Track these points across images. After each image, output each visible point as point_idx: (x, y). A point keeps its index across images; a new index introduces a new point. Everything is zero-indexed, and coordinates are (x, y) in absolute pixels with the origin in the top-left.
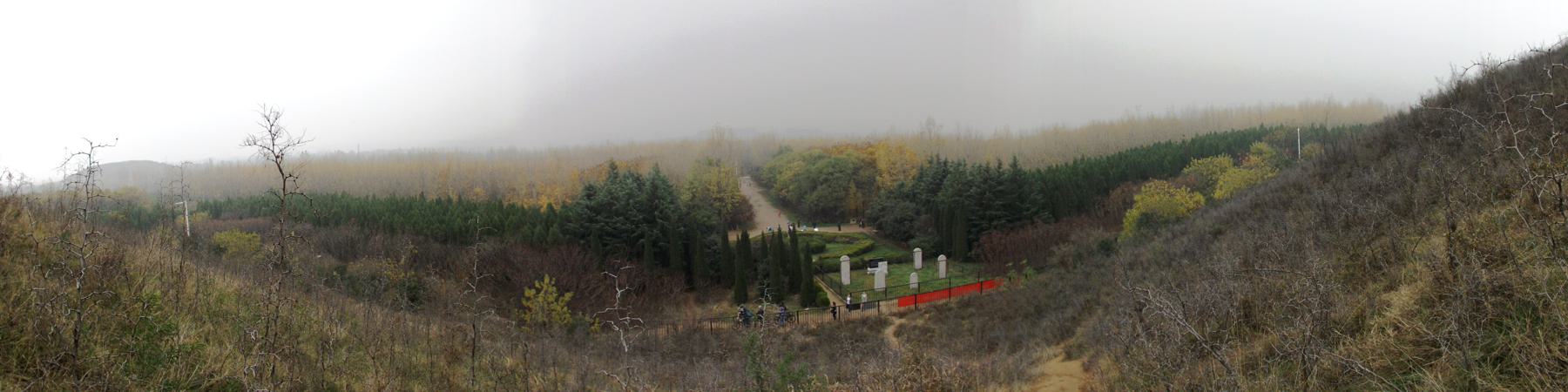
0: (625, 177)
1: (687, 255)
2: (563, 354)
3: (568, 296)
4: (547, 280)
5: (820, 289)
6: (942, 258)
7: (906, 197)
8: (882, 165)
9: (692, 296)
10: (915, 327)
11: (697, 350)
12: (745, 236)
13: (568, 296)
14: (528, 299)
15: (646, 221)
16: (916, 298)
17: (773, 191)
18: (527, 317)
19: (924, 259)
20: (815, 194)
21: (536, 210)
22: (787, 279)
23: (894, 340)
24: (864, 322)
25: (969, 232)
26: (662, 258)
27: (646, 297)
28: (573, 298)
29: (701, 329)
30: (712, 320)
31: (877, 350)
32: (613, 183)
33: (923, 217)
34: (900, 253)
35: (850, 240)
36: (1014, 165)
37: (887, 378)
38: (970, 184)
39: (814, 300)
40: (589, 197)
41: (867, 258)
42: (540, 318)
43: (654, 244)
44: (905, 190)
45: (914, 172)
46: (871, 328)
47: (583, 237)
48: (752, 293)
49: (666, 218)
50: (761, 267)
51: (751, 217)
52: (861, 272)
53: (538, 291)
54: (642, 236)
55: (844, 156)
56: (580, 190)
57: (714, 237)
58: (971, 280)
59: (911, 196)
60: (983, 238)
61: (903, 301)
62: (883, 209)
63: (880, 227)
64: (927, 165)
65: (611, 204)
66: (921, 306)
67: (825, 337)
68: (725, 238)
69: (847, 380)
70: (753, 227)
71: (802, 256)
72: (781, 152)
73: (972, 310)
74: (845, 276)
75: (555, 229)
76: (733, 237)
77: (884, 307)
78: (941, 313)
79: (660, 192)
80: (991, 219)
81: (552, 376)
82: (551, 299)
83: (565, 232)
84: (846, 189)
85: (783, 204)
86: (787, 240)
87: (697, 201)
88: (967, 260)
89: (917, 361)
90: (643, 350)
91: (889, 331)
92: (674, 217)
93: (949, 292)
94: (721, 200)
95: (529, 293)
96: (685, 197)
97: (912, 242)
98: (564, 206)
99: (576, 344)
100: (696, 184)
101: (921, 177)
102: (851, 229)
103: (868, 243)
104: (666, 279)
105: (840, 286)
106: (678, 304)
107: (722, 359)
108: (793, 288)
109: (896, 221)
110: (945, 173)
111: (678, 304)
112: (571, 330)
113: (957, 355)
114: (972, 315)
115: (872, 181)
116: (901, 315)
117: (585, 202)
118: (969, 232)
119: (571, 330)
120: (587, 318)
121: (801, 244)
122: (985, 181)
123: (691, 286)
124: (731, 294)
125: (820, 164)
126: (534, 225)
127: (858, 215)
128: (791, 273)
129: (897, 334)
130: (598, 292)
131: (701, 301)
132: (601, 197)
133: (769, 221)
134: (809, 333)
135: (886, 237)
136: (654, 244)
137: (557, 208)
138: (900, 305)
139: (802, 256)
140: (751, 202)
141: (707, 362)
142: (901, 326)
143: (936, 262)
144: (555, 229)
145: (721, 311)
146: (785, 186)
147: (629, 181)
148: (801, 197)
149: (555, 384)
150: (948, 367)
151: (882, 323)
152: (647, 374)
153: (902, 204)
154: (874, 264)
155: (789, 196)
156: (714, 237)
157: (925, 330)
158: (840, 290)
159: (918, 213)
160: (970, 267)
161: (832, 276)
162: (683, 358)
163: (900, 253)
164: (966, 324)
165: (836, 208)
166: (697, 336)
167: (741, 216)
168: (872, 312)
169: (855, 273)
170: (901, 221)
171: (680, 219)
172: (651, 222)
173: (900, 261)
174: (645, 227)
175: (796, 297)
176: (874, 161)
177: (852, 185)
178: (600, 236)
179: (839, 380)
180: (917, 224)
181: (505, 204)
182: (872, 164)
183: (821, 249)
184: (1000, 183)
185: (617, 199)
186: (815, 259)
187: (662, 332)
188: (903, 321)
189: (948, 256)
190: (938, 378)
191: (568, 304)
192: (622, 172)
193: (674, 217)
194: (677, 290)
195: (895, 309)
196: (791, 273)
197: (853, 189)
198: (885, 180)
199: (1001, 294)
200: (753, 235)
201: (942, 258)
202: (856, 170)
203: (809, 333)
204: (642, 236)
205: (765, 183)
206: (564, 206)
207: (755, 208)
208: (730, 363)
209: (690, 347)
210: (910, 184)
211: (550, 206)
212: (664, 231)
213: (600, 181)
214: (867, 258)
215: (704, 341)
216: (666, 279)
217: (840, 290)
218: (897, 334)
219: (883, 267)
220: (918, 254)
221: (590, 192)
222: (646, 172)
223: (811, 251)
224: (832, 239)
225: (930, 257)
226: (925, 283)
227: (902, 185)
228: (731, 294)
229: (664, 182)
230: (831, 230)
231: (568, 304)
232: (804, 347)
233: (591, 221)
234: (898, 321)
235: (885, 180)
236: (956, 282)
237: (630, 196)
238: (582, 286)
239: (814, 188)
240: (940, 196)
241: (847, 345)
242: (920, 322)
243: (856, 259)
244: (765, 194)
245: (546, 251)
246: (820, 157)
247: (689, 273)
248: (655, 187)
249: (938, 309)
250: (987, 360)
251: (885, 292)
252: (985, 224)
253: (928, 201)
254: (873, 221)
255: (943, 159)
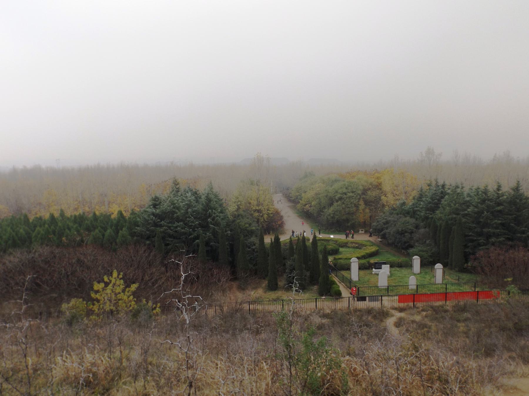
0: (186, 192)
1: (232, 251)
2: (128, 333)
3: (134, 287)
4: (115, 274)
5: (334, 283)
6: (439, 266)
7: (407, 213)
8: (387, 187)
9: (235, 284)
10: (413, 322)
11: (238, 325)
12: (277, 239)
13: (134, 287)
14: (97, 292)
15: (201, 225)
16: (414, 297)
17: (299, 206)
18: (96, 308)
19: (422, 265)
20: (332, 208)
21: (107, 217)
22: (308, 274)
23: (394, 331)
24: (369, 311)
25: (466, 246)
26: (212, 255)
27: (202, 283)
28: (138, 289)
29: (241, 310)
30: (250, 303)
31: (381, 335)
32: (175, 195)
33: (422, 230)
34: (402, 259)
35: (360, 246)
36: (517, 189)
37: (390, 359)
38: (467, 204)
39: (329, 291)
40: (155, 206)
41: (372, 261)
42: (108, 307)
43: (207, 244)
44: (407, 208)
45: (415, 193)
46: (375, 317)
47: (148, 238)
48: (281, 283)
49: (217, 224)
50: (289, 263)
51: (281, 225)
52: (368, 271)
53: (107, 284)
54: (197, 238)
55: (355, 180)
56: (147, 201)
57: (253, 239)
58: (467, 288)
59: (412, 213)
60: (480, 253)
61: (402, 298)
62: (387, 223)
63: (384, 237)
64: (425, 188)
65: (173, 213)
66: (419, 304)
67: (339, 320)
68: (262, 240)
69: (356, 355)
70: (283, 233)
71: (321, 257)
72: (306, 176)
73: (467, 315)
74: (355, 274)
75: (124, 231)
76: (268, 240)
77: (388, 302)
78: (438, 313)
79: (212, 204)
80: (489, 236)
81: (118, 354)
82: (118, 290)
83: (133, 234)
84: (357, 206)
85: (307, 215)
86: (309, 243)
87: (241, 212)
88: (463, 270)
89: (416, 349)
90: (196, 327)
91: (390, 322)
92: (223, 223)
93: (445, 296)
94: (259, 211)
95: (98, 286)
96: (232, 208)
97: (411, 251)
98: (133, 213)
99: (140, 326)
100: (241, 198)
101: (421, 196)
102: (361, 237)
103: (373, 249)
104: (215, 271)
105: (350, 281)
106: (224, 291)
107: (258, 332)
108: (313, 281)
109: (398, 232)
110: (443, 194)
111: (224, 291)
112: (136, 314)
113: (455, 352)
114: (466, 320)
115: (378, 200)
116: (401, 310)
117: (151, 210)
118: (466, 246)
119: (136, 314)
120: (150, 304)
121: (320, 248)
122: (483, 201)
123: (234, 277)
124: (265, 283)
125: (336, 186)
126: (105, 229)
127: (366, 226)
128: (313, 269)
129: (398, 324)
130: (160, 282)
131: (242, 289)
132: (165, 206)
133: (296, 227)
134: (325, 316)
135: (389, 245)
136: (207, 244)
137: (127, 215)
138: (400, 301)
139: (321, 257)
140: (282, 213)
141: (246, 334)
142: (400, 319)
143: (433, 269)
144: (124, 231)
145: (257, 298)
146: (309, 202)
147: (189, 194)
148: (321, 211)
149: (120, 361)
150: (444, 360)
151: (383, 314)
152: (199, 344)
153: (403, 219)
154: (378, 266)
155: (311, 210)
156: (253, 239)
157: (422, 325)
158: (349, 283)
159: (417, 227)
160: (465, 277)
161: (343, 273)
162: (227, 332)
163: (402, 259)
164: (462, 327)
165: (347, 220)
166: (238, 314)
167: (274, 224)
168: (375, 305)
169: (362, 272)
170: (402, 233)
171: (228, 225)
172: (205, 227)
173: (400, 266)
174: (200, 231)
175: (315, 288)
176: (380, 184)
177: (362, 202)
178: (163, 238)
179: (349, 354)
180: (416, 236)
181: (31, 218)
182: (378, 186)
183: (335, 252)
184: (499, 204)
185: (178, 208)
186: (330, 259)
187: (211, 312)
188: (402, 315)
189: (445, 265)
190: (435, 367)
191: (134, 294)
192: (182, 187)
193: (223, 223)
194: (223, 280)
195: (396, 305)
196: (313, 269)
197: (362, 206)
198: (389, 200)
199: (499, 305)
200: (284, 238)
201: (439, 266)
202: (365, 191)
203: (325, 316)
204: (197, 238)
205: (293, 201)
206: (133, 213)
207: (285, 219)
208: (263, 336)
209: (234, 323)
210: (410, 203)
211: (120, 213)
212: (215, 233)
213: (164, 194)
214: (372, 261)
215: (244, 318)
216: (215, 271)
217: (349, 283)
218: (398, 324)
219: (386, 269)
220: (416, 261)
221: (156, 202)
222: (202, 188)
223: (327, 253)
224: (345, 245)
225: (428, 264)
226: (423, 286)
227: (404, 204)
228: (265, 283)
229: (216, 196)
230: (342, 237)
231: (134, 294)
232: (321, 327)
233: (156, 225)
234: (398, 315)
235: (389, 200)
236: (451, 289)
237: (189, 206)
238: (147, 278)
239: (331, 204)
240: (438, 213)
241: (356, 328)
242: (418, 318)
243: (363, 261)
244: (294, 208)
245: (115, 251)
246: (336, 181)
247: (233, 265)
248: (209, 200)
249: (435, 310)
250: (485, 362)
251: (388, 289)
252: (482, 240)
253: (427, 218)
254: (378, 231)
255: (441, 183)
